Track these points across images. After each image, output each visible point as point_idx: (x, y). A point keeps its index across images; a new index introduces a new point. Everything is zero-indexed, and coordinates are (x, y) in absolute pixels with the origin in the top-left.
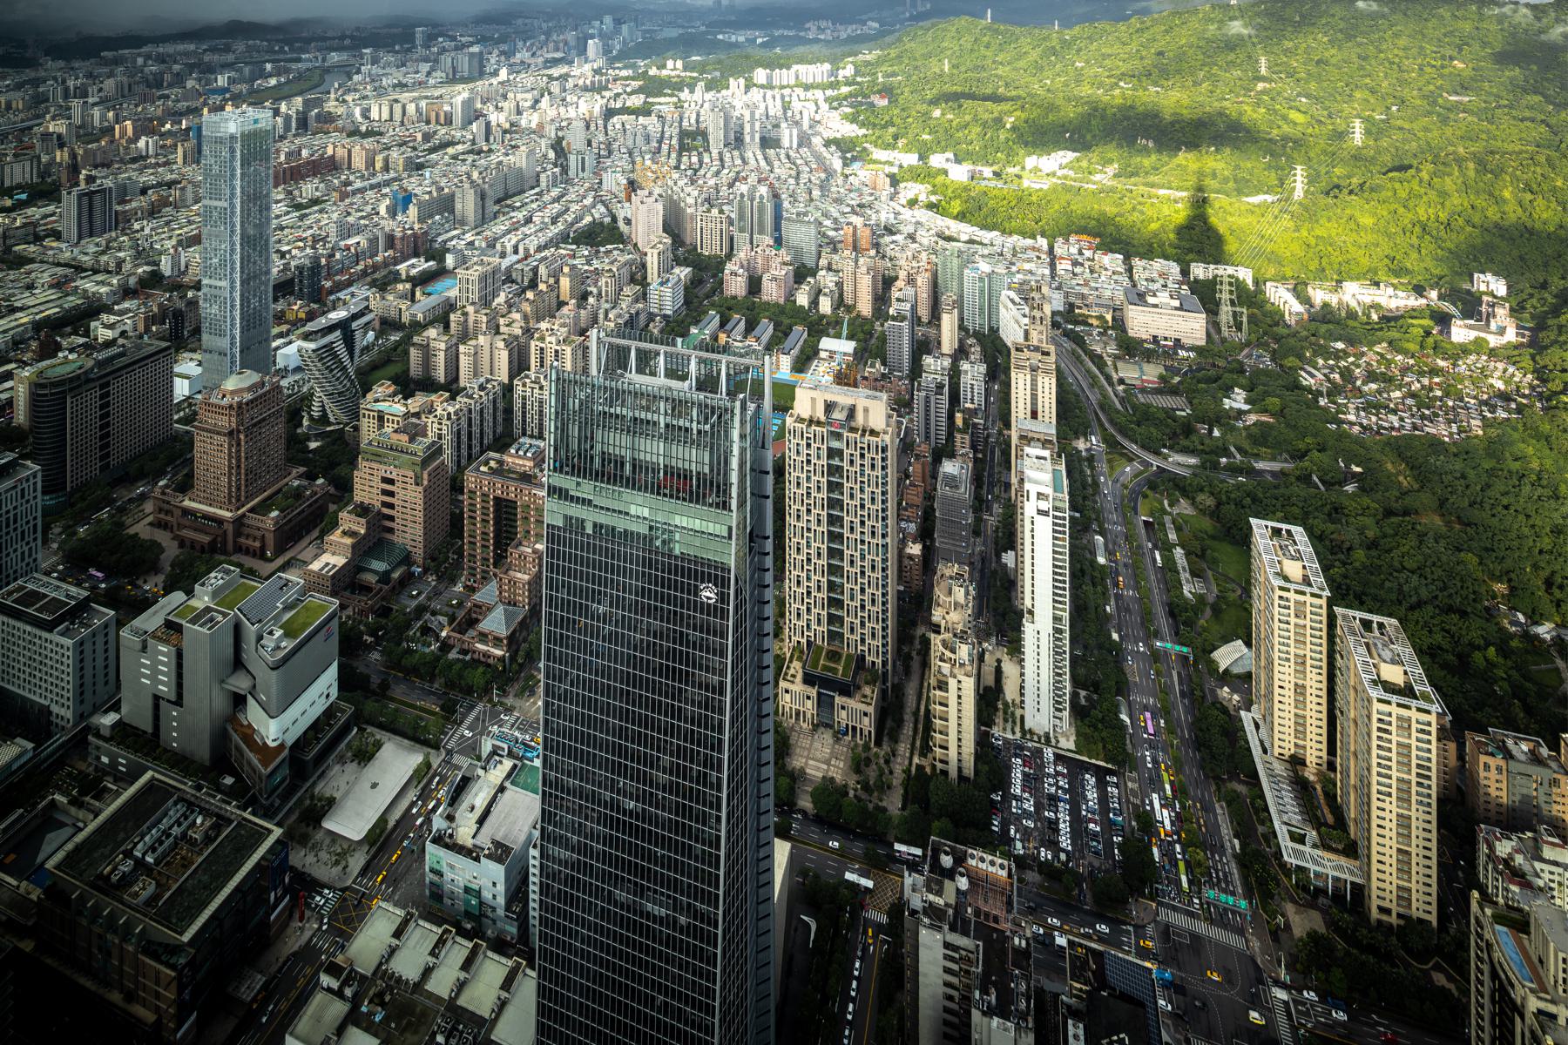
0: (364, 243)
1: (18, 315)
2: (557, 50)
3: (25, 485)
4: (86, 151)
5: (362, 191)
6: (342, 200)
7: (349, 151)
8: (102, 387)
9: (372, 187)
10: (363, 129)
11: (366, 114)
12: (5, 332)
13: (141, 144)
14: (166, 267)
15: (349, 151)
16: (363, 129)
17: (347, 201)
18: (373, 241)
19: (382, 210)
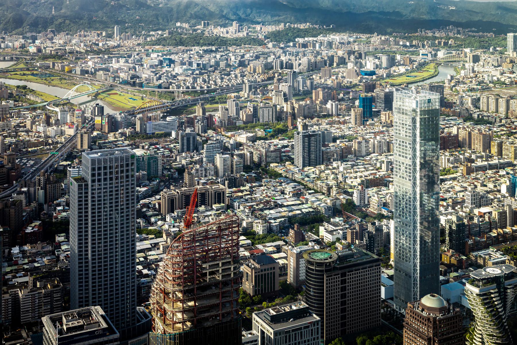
0: (495, 215)
1: (280, 209)
2: (367, 170)
3: (313, 328)
4: (299, 105)
5: (483, 169)
6: (468, 173)
7: (470, 134)
8: (343, 275)
9: (491, 167)
10: (475, 116)
11: (476, 102)
12: (483, 343)
13: (328, 106)
14: (356, 198)
15: (470, 134)
16: (475, 116)
17: (473, 175)
18: (502, 215)
19: (504, 189)
